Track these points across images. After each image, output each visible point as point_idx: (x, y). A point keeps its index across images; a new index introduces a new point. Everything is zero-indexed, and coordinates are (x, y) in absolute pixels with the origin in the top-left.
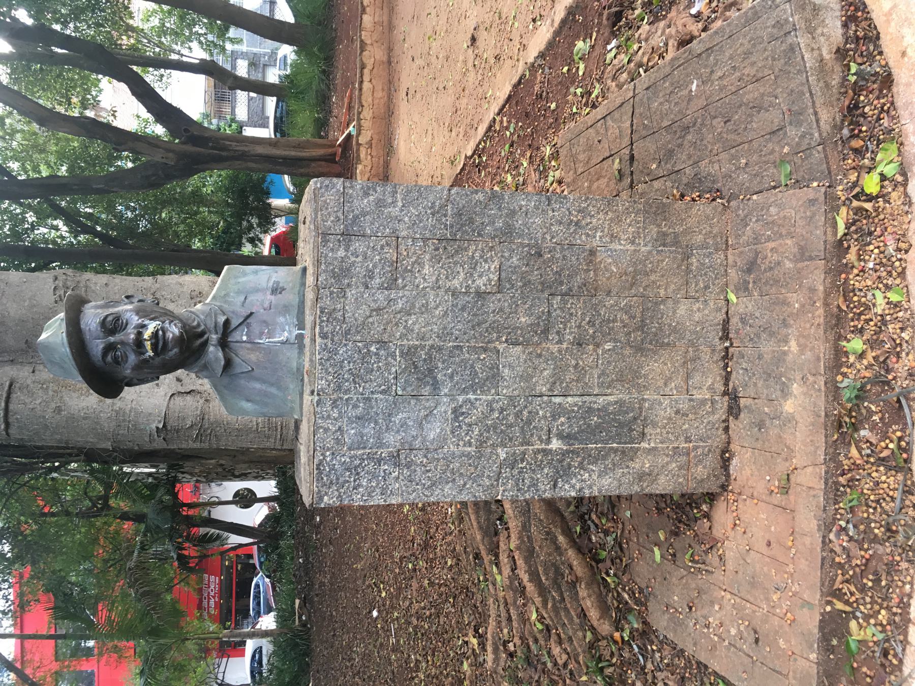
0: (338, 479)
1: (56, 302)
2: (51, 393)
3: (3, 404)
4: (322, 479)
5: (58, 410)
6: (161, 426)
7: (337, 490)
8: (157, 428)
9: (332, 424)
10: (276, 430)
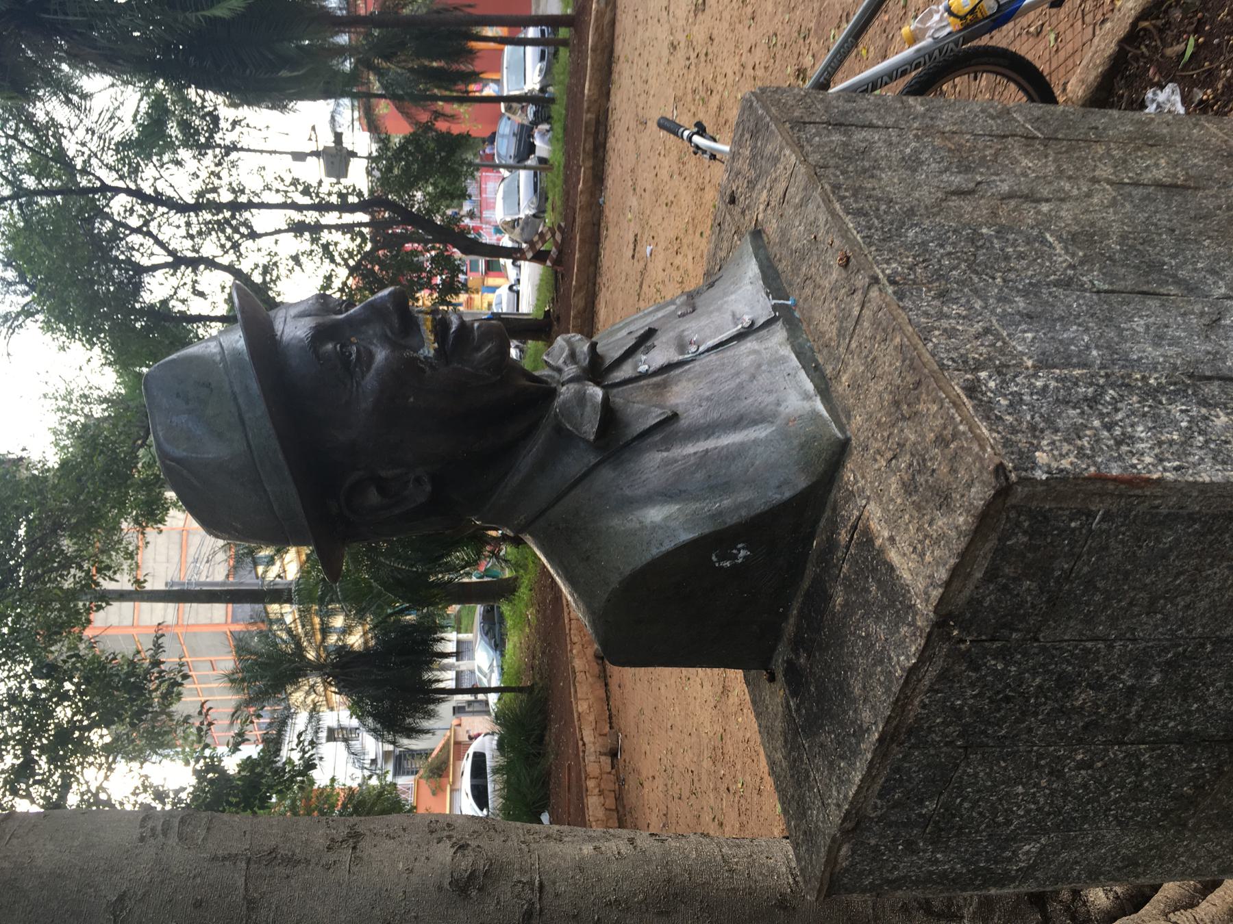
1: (142, 839)
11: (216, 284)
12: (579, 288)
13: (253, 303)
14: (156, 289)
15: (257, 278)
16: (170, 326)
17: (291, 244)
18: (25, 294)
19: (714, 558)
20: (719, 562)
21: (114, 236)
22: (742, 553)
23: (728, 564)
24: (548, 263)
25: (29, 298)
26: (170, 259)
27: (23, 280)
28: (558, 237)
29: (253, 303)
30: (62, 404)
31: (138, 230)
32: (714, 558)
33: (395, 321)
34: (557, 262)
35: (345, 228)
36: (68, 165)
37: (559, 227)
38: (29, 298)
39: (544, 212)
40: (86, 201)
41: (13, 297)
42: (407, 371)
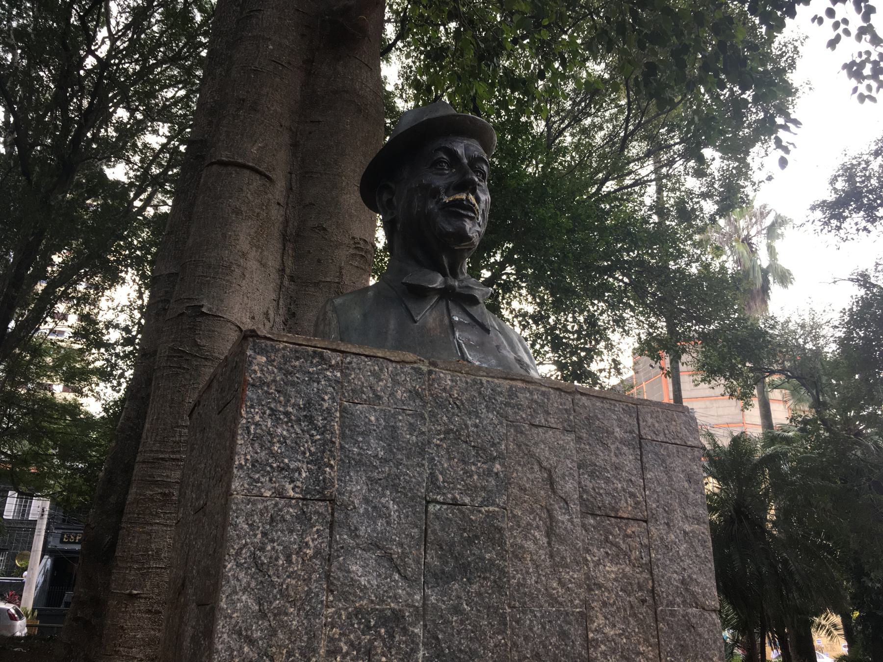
0: (293, 384)
1: (353, 238)
2: (257, 210)
3: (250, 164)
4: (297, 358)
5: (238, 212)
6: (204, 310)
7: (274, 381)
8: (202, 306)
9: (386, 386)
10: (173, 453)
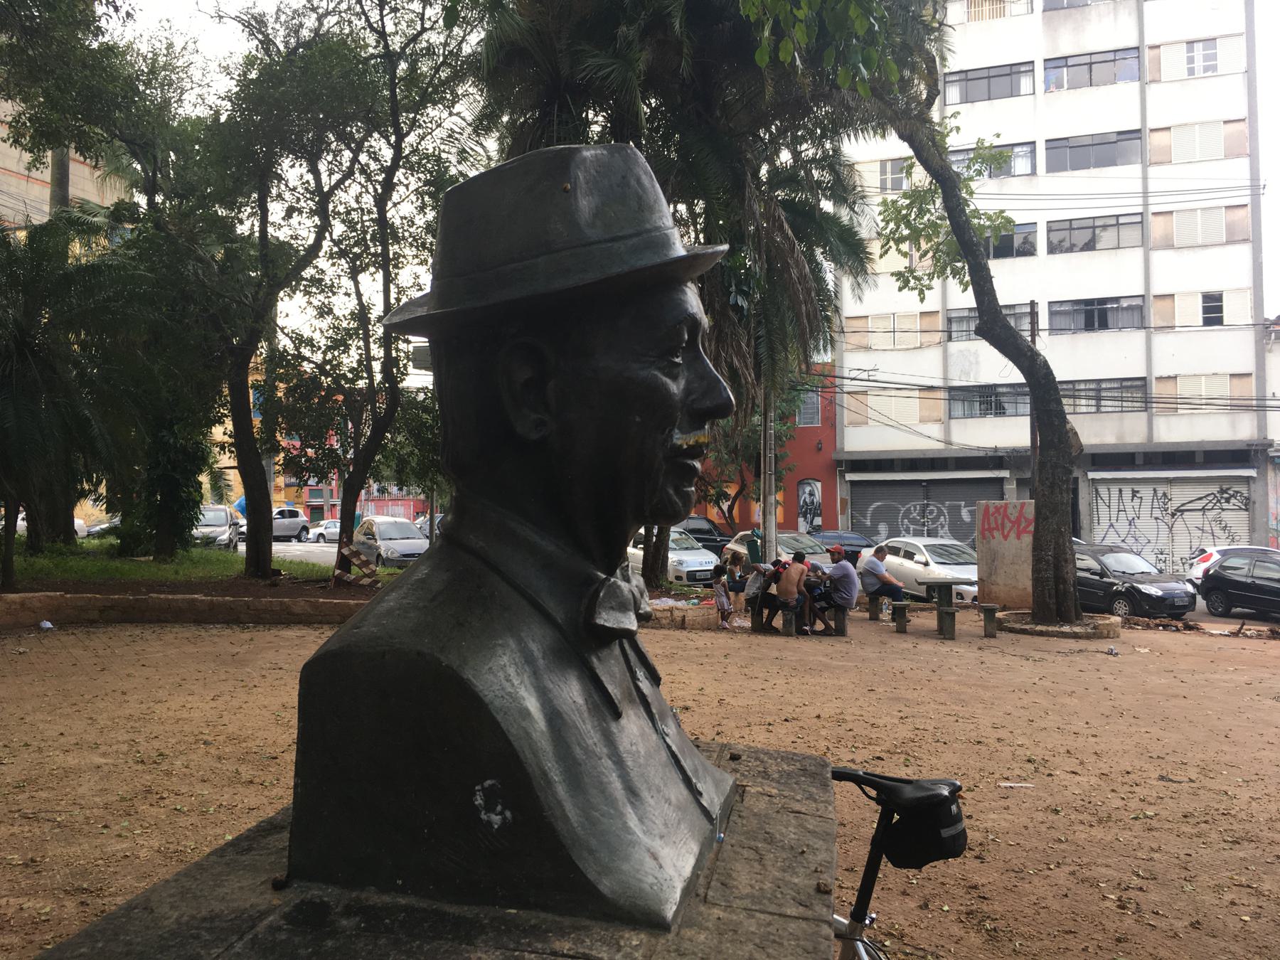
11: (302, 229)
12: (316, 606)
13: (283, 267)
14: (293, 171)
15: (308, 272)
16: (262, 180)
17: (344, 305)
18: (286, 43)
19: (488, 783)
20: (483, 789)
21: (345, 139)
22: (496, 819)
23: (479, 801)
24: (338, 572)
25: (282, 47)
26: (326, 189)
27: (299, 45)
28: (366, 581)
29: (283, 267)
30: (162, 60)
31: (355, 160)
32: (488, 783)
33: (708, 403)
34: (338, 580)
35: (366, 360)
36: (418, 107)
37: (377, 582)
38: (282, 47)
39: (383, 564)
40: (390, 119)
41: (282, 33)
42: (661, 411)
